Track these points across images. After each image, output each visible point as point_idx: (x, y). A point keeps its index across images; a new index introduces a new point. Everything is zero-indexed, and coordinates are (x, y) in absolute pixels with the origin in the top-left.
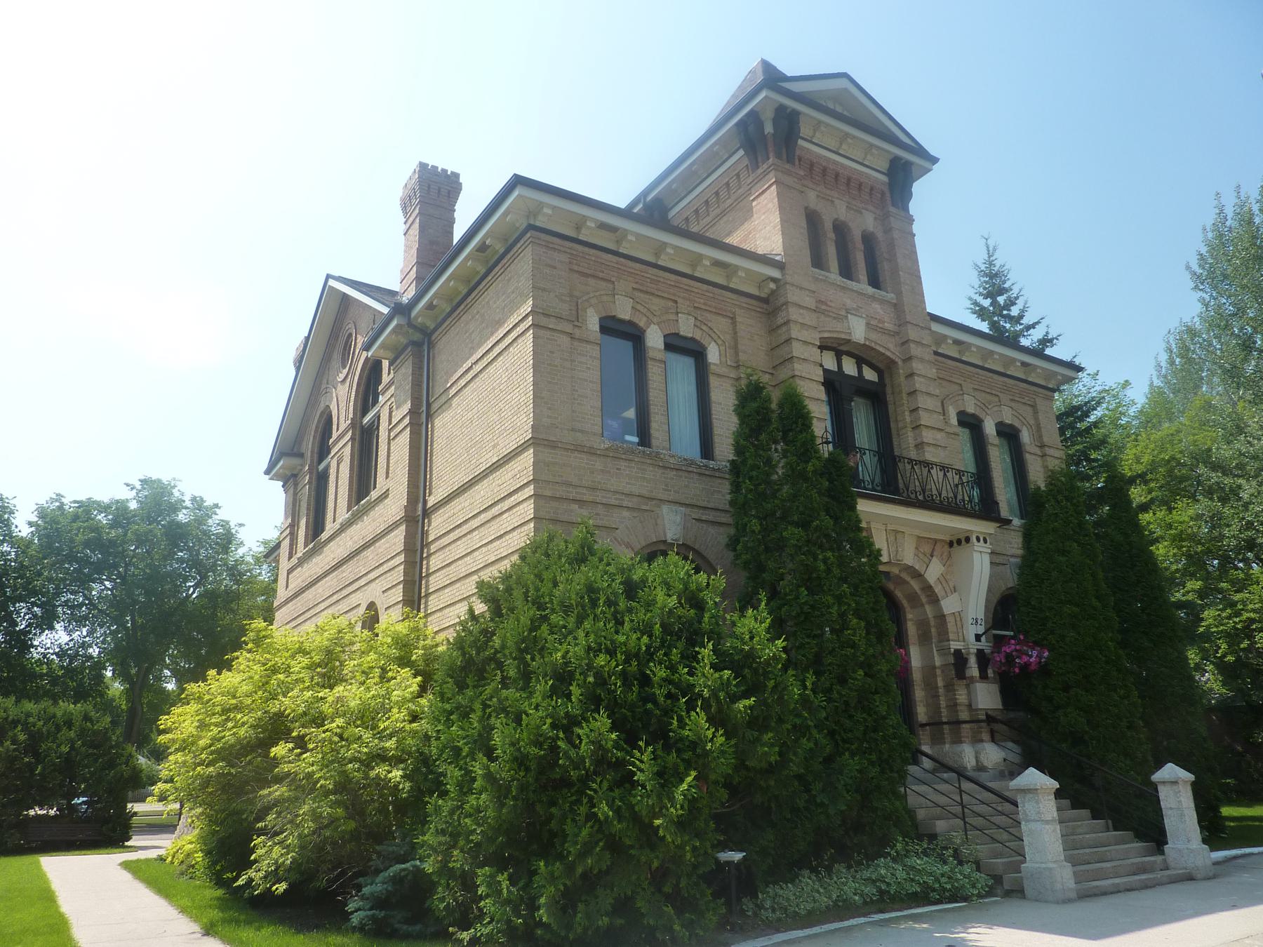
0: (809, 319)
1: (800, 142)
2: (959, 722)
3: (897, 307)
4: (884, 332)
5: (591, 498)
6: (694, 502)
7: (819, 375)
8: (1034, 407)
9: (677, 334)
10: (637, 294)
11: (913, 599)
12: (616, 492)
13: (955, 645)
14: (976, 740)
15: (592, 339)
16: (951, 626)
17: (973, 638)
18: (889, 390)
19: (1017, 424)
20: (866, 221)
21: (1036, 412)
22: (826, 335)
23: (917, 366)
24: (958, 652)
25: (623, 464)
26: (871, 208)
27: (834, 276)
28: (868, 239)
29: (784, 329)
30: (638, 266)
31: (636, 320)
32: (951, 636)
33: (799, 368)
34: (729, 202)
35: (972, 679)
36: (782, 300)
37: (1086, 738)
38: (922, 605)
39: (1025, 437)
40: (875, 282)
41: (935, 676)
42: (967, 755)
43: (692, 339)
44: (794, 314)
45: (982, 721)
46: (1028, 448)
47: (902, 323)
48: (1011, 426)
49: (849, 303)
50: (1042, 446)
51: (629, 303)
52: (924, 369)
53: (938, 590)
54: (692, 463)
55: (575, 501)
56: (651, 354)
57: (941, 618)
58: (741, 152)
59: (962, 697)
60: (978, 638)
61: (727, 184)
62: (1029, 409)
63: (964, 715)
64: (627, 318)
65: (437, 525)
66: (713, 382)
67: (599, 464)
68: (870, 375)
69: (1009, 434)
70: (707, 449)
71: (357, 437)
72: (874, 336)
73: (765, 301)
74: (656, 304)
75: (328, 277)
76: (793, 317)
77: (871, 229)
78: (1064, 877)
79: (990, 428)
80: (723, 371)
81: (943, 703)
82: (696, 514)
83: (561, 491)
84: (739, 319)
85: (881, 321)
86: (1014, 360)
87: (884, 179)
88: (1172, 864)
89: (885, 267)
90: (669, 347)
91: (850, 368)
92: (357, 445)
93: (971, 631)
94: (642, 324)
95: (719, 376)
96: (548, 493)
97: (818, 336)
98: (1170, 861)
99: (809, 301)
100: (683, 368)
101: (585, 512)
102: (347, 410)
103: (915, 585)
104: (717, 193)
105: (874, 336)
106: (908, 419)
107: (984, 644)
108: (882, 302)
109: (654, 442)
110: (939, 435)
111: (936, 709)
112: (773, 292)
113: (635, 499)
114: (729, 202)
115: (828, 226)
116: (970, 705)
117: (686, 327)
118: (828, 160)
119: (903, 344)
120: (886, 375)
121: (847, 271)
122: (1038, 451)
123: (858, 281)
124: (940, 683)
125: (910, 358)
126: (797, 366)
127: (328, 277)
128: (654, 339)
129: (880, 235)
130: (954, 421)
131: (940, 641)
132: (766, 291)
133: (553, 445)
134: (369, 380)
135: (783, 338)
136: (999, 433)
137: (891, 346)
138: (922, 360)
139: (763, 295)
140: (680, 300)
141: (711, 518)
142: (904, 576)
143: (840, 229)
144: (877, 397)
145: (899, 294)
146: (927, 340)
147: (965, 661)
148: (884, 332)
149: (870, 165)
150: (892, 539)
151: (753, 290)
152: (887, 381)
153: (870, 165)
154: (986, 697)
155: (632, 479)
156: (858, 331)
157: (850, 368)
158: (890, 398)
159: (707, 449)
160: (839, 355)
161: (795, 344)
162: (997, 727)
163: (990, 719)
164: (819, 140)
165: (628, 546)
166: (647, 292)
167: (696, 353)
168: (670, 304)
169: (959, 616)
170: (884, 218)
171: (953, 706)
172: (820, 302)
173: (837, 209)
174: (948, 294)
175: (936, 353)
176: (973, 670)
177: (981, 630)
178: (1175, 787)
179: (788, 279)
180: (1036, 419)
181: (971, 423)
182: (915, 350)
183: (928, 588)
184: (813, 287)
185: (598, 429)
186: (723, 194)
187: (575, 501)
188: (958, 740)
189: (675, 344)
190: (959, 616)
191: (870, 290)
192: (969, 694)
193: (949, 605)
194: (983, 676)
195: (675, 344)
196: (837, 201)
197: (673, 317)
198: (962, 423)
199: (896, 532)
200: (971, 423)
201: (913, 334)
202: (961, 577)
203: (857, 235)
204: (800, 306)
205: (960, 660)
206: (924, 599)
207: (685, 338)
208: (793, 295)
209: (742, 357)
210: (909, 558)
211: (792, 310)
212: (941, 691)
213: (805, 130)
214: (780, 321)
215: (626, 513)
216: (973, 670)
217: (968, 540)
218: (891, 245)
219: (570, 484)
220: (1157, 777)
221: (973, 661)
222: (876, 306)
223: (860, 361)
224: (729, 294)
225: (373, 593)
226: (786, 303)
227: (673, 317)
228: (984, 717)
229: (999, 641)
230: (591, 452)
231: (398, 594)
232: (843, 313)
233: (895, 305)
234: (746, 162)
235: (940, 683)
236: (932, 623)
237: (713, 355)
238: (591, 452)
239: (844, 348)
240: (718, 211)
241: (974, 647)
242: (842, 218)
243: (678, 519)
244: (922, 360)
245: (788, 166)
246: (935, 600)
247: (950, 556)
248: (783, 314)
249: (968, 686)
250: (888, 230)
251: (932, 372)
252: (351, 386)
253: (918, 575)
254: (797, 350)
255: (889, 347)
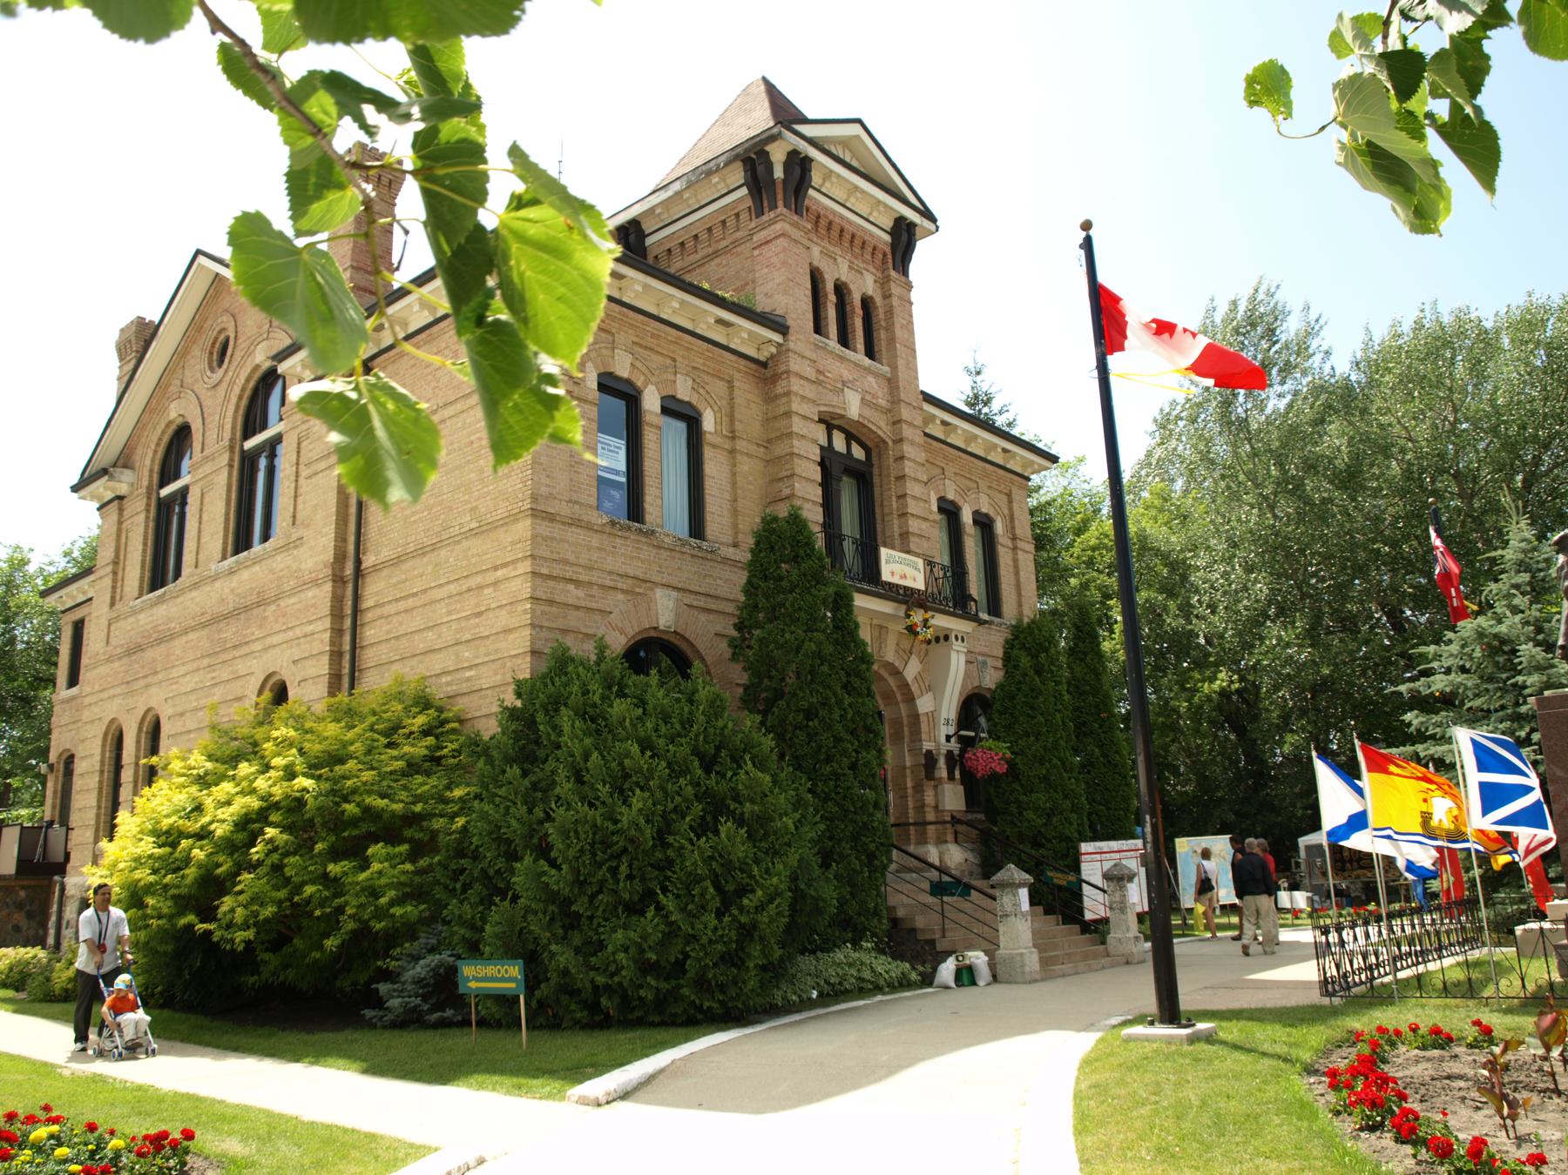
0: (809, 391)
1: (811, 192)
2: (926, 823)
3: (892, 383)
4: (876, 407)
5: (586, 579)
6: (686, 586)
7: (815, 454)
8: (1009, 495)
9: (673, 397)
10: (637, 349)
11: (889, 696)
12: (611, 573)
13: (927, 745)
14: (940, 841)
15: (590, 398)
16: (924, 727)
17: (943, 739)
18: (875, 471)
19: (992, 514)
20: (864, 284)
21: (1010, 501)
22: (823, 409)
23: (908, 449)
24: (929, 752)
25: (618, 541)
26: (871, 268)
27: (833, 343)
28: (866, 303)
29: (784, 400)
30: (641, 317)
31: (634, 379)
32: (924, 736)
33: (799, 446)
34: (724, 243)
36: (783, 368)
38: (897, 703)
39: (999, 527)
40: (870, 353)
41: (905, 776)
43: (689, 403)
44: (796, 385)
45: (945, 822)
46: (1001, 540)
47: (895, 400)
48: (986, 515)
49: (846, 375)
50: (1014, 538)
51: (628, 359)
52: (914, 452)
53: (914, 688)
54: (684, 543)
55: (571, 580)
56: (648, 418)
57: (915, 717)
58: (744, 191)
59: (929, 798)
60: (948, 738)
61: (724, 222)
62: (1005, 498)
63: (930, 817)
64: (625, 374)
65: (374, 591)
66: (708, 453)
67: (595, 540)
68: (858, 453)
69: (984, 523)
70: (697, 526)
71: (236, 464)
72: (867, 413)
73: (764, 365)
74: (656, 361)
75: (198, 252)
76: (795, 388)
77: (870, 293)
78: (1032, 961)
79: (967, 517)
80: (718, 440)
81: (911, 804)
82: (689, 599)
83: (557, 570)
84: (737, 384)
85: (875, 396)
86: (995, 446)
87: (888, 238)
89: (881, 336)
90: (666, 411)
91: (839, 443)
92: (235, 473)
93: (945, 730)
94: (639, 384)
95: (714, 446)
96: (544, 571)
97: (816, 410)
98: (1111, 949)
99: (809, 372)
100: (676, 431)
101: (581, 593)
102: (221, 427)
103: (891, 681)
104: (710, 230)
105: (867, 413)
106: (895, 505)
107: (954, 745)
108: (877, 375)
109: (648, 518)
110: (924, 525)
112: (772, 356)
113: (630, 581)
114: (724, 243)
115: (830, 287)
116: (936, 807)
117: (684, 391)
118: (834, 213)
119: (894, 423)
120: (874, 454)
121: (844, 340)
123: (855, 350)
124: (909, 784)
125: (901, 440)
126: (796, 443)
127: (198, 252)
128: (651, 402)
129: (878, 300)
130: (935, 508)
131: (912, 741)
132: (767, 354)
133: (551, 518)
134: (256, 391)
135: (782, 410)
136: (975, 522)
137: (882, 424)
138: (912, 443)
139: (762, 359)
140: (679, 359)
141: (702, 604)
143: (841, 290)
144: (863, 477)
145: (894, 368)
146: (918, 421)
147: (936, 761)
148: (876, 407)
149: (872, 214)
151: (752, 352)
152: (875, 460)
153: (872, 214)
154: (952, 798)
155: (625, 556)
156: (853, 407)
157: (839, 443)
158: (876, 480)
159: (697, 526)
160: (830, 428)
161: (795, 419)
162: (960, 828)
163: (955, 820)
164: (833, 187)
165: (622, 632)
166: (646, 348)
167: (691, 419)
168: (669, 362)
170: (884, 282)
171: (921, 807)
172: (819, 371)
173: (838, 269)
174: (940, 372)
175: (926, 435)
176: (942, 771)
177: (952, 731)
179: (791, 345)
181: (950, 511)
182: (907, 432)
183: (905, 686)
184: (814, 356)
185: (593, 501)
186: (717, 232)
187: (571, 580)
188: (923, 840)
189: (671, 408)
190: (933, 716)
191: (867, 361)
192: (936, 795)
193: (924, 704)
194: (951, 777)
195: (671, 408)
196: (839, 259)
197: (671, 377)
198: (941, 510)
199: (881, 627)
200: (950, 511)
201: (905, 413)
202: (944, 675)
203: (856, 298)
204: (802, 377)
205: (930, 758)
206: (899, 697)
207: (681, 401)
208: (795, 365)
209: (738, 426)
210: (890, 655)
211: (793, 380)
212: (910, 791)
213: (816, 178)
214: (779, 390)
215: (620, 596)
216: (942, 771)
217: (946, 638)
218: (890, 312)
219: (565, 562)
221: (942, 763)
222: (871, 379)
223: (850, 437)
224: (728, 355)
225: (280, 662)
226: (787, 372)
227: (671, 377)
229: (967, 743)
230: (589, 527)
231: (323, 667)
232: (839, 385)
233: (889, 380)
234: (749, 203)
235: (909, 784)
236: (905, 722)
237: (708, 423)
238: (589, 527)
239: (836, 422)
240: (710, 250)
241: (945, 747)
242: (844, 279)
243: (671, 604)
244: (912, 443)
245: (796, 218)
246: (910, 699)
247: (927, 654)
248: (784, 383)
249: (935, 787)
250: (887, 296)
251: (921, 456)
252: (226, 398)
253: (896, 673)
254: (798, 425)
255: (880, 425)
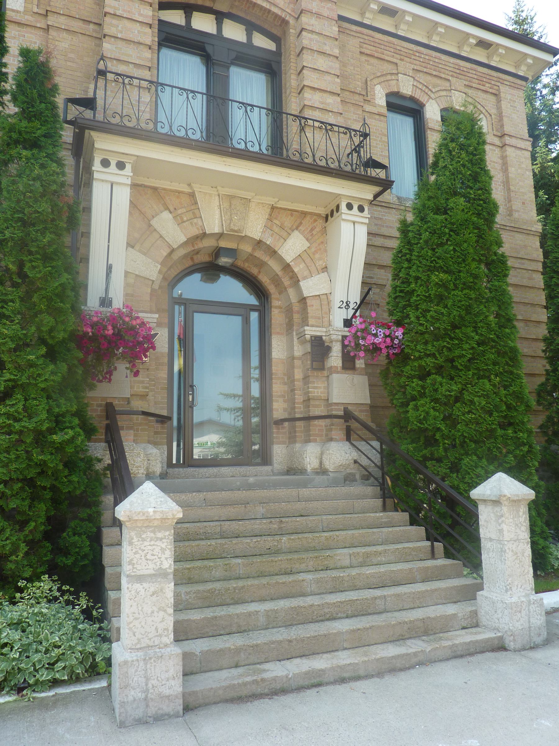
13: (310, 331)
21: (499, 101)
35: (332, 370)
37: (438, 436)
42: (310, 456)
62: (493, 99)
68: (261, 41)
80: (28, 19)
88: (484, 620)
93: (338, 317)
95: (19, 24)
111: (292, 402)
122: (497, 141)
142: (259, 254)
150: (226, 205)
169: (325, 299)
178: (497, 509)
180: (499, 108)
183: (287, 267)
190: (325, 299)
193: (311, 286)
205: (319, 348)
216: (335, 358)
220: (475, 493)
221: (336, 351)
228: (341, 413)
